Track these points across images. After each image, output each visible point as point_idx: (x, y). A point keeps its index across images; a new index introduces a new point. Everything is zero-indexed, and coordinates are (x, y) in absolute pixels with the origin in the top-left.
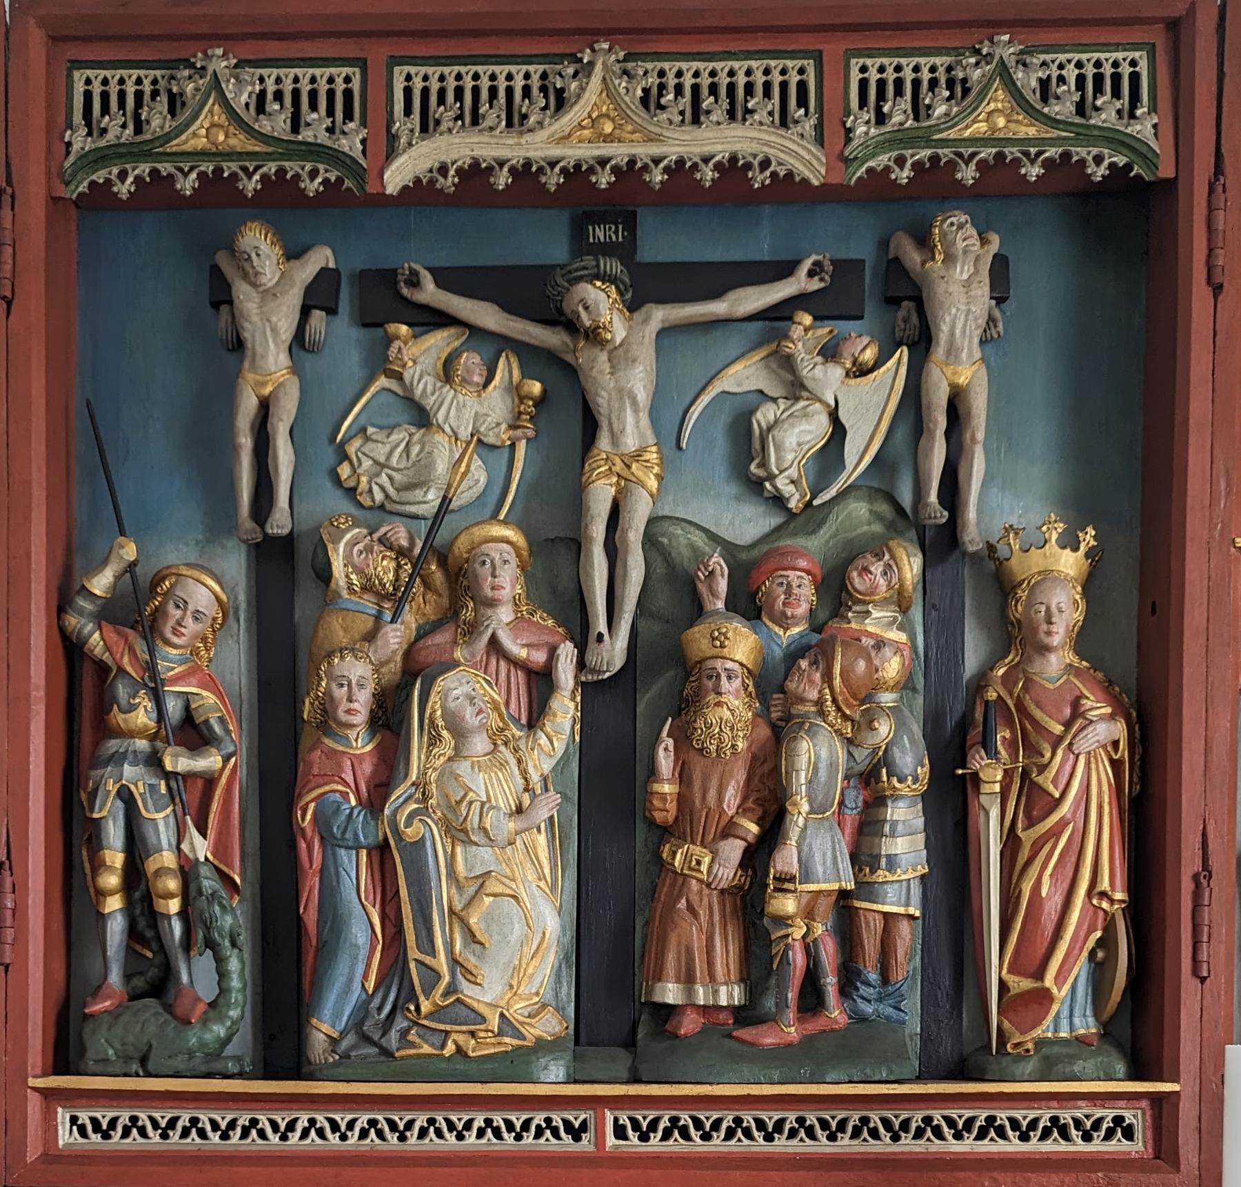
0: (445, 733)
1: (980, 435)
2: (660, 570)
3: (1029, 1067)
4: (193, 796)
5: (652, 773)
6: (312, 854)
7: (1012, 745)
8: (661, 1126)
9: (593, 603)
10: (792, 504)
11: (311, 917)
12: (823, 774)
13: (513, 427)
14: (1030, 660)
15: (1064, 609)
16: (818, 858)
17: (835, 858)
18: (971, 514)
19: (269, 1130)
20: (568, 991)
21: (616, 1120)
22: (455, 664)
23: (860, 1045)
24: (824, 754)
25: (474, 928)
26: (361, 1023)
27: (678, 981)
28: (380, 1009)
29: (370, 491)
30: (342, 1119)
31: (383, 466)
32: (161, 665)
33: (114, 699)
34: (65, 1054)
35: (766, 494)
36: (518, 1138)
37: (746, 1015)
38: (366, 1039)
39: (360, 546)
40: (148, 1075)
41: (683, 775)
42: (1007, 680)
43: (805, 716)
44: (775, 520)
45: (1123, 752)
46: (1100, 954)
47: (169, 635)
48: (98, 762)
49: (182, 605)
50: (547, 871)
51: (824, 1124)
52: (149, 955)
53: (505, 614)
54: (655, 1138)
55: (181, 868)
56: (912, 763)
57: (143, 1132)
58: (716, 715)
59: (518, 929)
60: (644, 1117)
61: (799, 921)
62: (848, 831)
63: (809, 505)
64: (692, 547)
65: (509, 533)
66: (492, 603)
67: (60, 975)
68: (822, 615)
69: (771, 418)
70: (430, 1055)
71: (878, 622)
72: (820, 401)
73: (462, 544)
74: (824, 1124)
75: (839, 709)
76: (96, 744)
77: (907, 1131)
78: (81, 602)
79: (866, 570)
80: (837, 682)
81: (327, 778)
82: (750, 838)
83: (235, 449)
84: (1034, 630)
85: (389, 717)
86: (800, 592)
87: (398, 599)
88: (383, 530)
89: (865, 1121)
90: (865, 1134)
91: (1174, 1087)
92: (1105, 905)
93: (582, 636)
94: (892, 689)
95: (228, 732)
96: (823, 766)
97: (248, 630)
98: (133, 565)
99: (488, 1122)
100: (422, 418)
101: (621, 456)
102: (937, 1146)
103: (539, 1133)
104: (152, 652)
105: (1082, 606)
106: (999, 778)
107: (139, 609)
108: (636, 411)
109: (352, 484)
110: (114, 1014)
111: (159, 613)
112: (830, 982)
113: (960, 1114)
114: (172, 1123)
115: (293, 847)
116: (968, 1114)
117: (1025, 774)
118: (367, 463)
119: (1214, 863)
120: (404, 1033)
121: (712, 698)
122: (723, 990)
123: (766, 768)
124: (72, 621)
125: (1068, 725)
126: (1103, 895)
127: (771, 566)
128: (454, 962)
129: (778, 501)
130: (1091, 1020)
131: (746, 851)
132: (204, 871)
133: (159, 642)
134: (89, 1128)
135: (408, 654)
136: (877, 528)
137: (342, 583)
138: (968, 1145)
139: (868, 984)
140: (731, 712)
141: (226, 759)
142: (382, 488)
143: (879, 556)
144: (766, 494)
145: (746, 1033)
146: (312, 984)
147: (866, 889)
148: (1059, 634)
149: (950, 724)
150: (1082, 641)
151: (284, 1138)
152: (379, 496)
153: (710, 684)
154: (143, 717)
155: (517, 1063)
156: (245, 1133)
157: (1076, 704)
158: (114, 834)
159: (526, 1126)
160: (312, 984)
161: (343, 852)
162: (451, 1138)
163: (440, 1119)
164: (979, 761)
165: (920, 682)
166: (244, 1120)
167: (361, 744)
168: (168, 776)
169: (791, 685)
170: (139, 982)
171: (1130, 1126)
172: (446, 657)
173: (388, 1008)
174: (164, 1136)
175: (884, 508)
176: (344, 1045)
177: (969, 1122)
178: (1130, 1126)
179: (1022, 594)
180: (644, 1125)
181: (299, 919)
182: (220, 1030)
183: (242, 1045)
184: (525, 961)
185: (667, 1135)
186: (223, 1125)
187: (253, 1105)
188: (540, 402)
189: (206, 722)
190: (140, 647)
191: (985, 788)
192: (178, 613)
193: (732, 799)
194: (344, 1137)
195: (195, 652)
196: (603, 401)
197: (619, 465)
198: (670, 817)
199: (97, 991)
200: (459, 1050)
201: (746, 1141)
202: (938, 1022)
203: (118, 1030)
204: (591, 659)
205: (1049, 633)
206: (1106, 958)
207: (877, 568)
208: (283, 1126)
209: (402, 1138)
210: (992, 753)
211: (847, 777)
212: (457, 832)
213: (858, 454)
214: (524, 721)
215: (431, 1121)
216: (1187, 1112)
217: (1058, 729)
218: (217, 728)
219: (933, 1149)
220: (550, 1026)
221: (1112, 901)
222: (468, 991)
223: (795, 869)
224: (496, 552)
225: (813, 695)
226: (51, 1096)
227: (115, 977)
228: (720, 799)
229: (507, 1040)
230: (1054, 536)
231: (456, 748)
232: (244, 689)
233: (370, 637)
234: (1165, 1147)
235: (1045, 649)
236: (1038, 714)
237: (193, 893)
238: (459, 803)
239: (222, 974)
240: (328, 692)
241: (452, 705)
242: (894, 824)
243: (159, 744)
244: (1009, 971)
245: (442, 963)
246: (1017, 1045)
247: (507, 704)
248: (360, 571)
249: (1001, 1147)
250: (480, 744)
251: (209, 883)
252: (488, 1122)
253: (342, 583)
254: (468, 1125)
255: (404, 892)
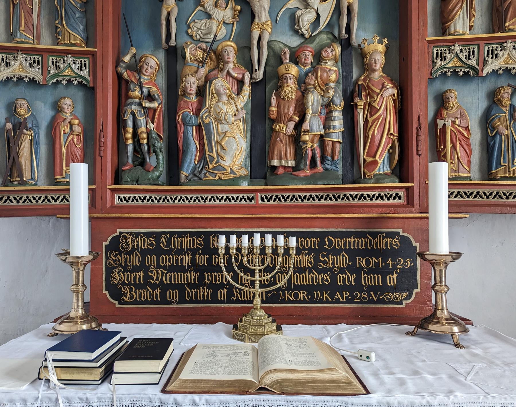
0: (215, 95)
1: (356, 15)
2: (272, 54)
3: (372, 181)
4: (151, 115)
5: (270, 105)
6: (181, 128)
7: (366, 96)
8: (273, 198)
9: (254, 62)
10: (306, 36)
11: (181, 145)
12: (315, 103)
13: (233, 18)
14: (370, 74)
15: (379, 60)
16: (314, 126)
17: (319, 126)
18: (354, 36)
19: (170, 200)
20: (248, 163)
21: (261, 196)
22: (218, 78)
23: (327, 175)
24: (316, 98)
25: (223, 145)
26: (194, 172)
27: (277, 159)
28: (199, 168)
29: (196, 36)
30: (189, 196)
31: (199, 29)
32: (142, 80)
33: (130, 89)
34: (117, 180)
35: (299, 34)
36: (235, 201)
37: (295, 169)
38: (195, 175)
39: (193, 49)
40: (138, 185)
41: (278, 106)
42: (364, 80)
43: (310, 89)
44: (302, 41)
45: (396, 97)
46: (391, 151)
47: (144, 72)
48: (126, 105)
49: (147, 64)
50: (243, 132)
51: (317, 197)
52: (139, 156)
53: (231, 65)
54: (272, 201)
55: (147, 132)
56: (339, 102)
57: (137, 200)
58: (287, 89)
59: (235, 146)
60: (269, 195)
61: (310, 143)
62: (322, 120)
63: (311, 36)
64: (280, 48)
65: (232, 44)
66: (228, 63)
67: (116, 161)
68: (314, 64)
69: (301, 14)
70: (212, 179)
71: (329, 65)
72: (313, 9)
73: (220, 47)
74: (317, 197)
75: (319, 86)
76: (126, 101)
77: (339, 198)
78: (122, 64)
79: (326, 51)
80: (319, 79)
81: (185, 108)
82: (296, 121)
83: (161, 25)
84: (371, 65)
85: (201, 92)
86: (309, 57)
87: (203, 62)
88: (199, 45)
89: (328, 195)
90: (328, 199)
91: (413, 185)
92: (392, 137)
93: (251, 70)
94: (334, 82)
95: (160, 98)
96: (315, 101)
97: (165, 72)
98: (135, 54)
99: (227, 197)
100: (209, 16)
101: (261, 23)
102: (348, 202)
103: (241, 200)
104: (140, 77)
105: (384, 59)
106: (363, 104)
107: (137, 67)
108: (265, 11)
109: (191, 34)
110: (130, 170)
111: (142, 67)
112: (318, 160)
113: (354, 193)
114: (145, 198)
115: (176, 127)
116: (356, 193)
117: (370, 104)
118: (195, 29)
119: (422, 124)
120: (205, 174)
121: (286, 84)
122: (290, 162)
123: (300, 103)
124: (119, 69)
125: (381, 90)
126: (391, 134)
127: (300, 50)
128: (218, 155)
129: (303, 35)
130: (389, 169)
131: (295, 125)
132: (153, 132)
133: (142, 75)
134: (123, 199)
135: (206, 77)
136: (329, 41)
137: (189, 58)
138: (356, 201)
139: (328, 160)
140: (290, 89)
141: (159, 104)
142: (199, 35)
143: (329, 47)
144: (299, 34)
145: (296, 173)
146: (182, 159)
147: (327, 135)
148: (378, 67)
149: (349, 92)
150: (384, 69)
151: (174, 202)
152: (198, 37)
153: (285, 81)
154: (137, 93)
155: (235, 181)
156: (164, 201)
157: (383, 84)
158: (130, 123)
159: (237, 198)
160: (182, 159)
161: (189, 127)
162: (218, 201)
163: (215, 196)
164: (357, 100)
165: (341, 81)
166: (163, 197)
167: (193, 99)
168: (144, 108)
169: (307, 80)
170: (136, 163)
171: (400, 196)
172: (216, 76)
173: (201, 167)
174: (143, 201)
175: (330, 36)
176: (190, 177)
177: (356, 196)
178: (400, 196)
179: (368, 56)
180: (269, 198)
181: (178, 145)
182: (157, 174)
183: (163, 178)
184: (237, 155)
185: (275, 200)
186: (158, 199)
187: (165, 193)
188: (240, 12)
189: (154, 95)
190: (137, 76)
191: (359, 107)
192: (147, 66)
193: (291, 110)
194: (189, 201)
195: (151, 78)
196: (256, 9)
197: (261, 26)
198: (275, 116)
199: (125, 165)
200: (220, 178)
201: (296, 201)
202: (347, 171)
203: (131, 173)
204: (254, 76)
205: (375, 66)
206: (392, 152)
207: (329, 50)
208: (173, 199)
209: (205, 202)
210: (360, 98)
211: (322, 106)
212: (219, 121)
213: (324, 22)
214: (236, 93)
215: (212, 197)
216: (416, 192)
217: (378, 91)
218: (157, 97)
219: (347, 203)
220: (243, 172)
221: (394, 136)
222: (222, 162)
223: (308, 128)
224: (229, 49)
225: (313, 82)
226: (113, 190)
227: (130, 161)
228: (288, 111)
229: (232, 175)
230: (376, 40)
231: (219, 100)
232: (164, 88)
233: (196, 72)
234: (410, 201)
235: (375, 71)
236: (373, 88)
237: (150, 138)
238: (219, 113)
239: (158, 159)
240: (185, 86)
241: (217, 87)
242: (335, 117)
243: (141, 100)
244: (367, 156)
245: (215, 155)
246: (369, 176)
247: (232, 89)
248: (193, 55)
249: (365, 202)
250: (224, 98)
251: (154, 136)
252: (227, 197)
253: (189, 58)
254: (222, 198)
255: (205, 137)
